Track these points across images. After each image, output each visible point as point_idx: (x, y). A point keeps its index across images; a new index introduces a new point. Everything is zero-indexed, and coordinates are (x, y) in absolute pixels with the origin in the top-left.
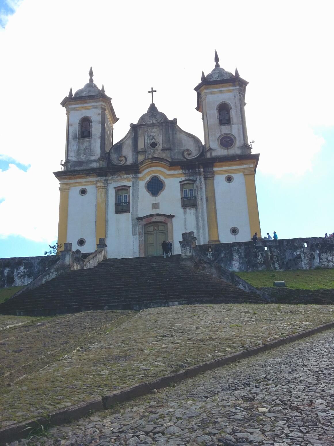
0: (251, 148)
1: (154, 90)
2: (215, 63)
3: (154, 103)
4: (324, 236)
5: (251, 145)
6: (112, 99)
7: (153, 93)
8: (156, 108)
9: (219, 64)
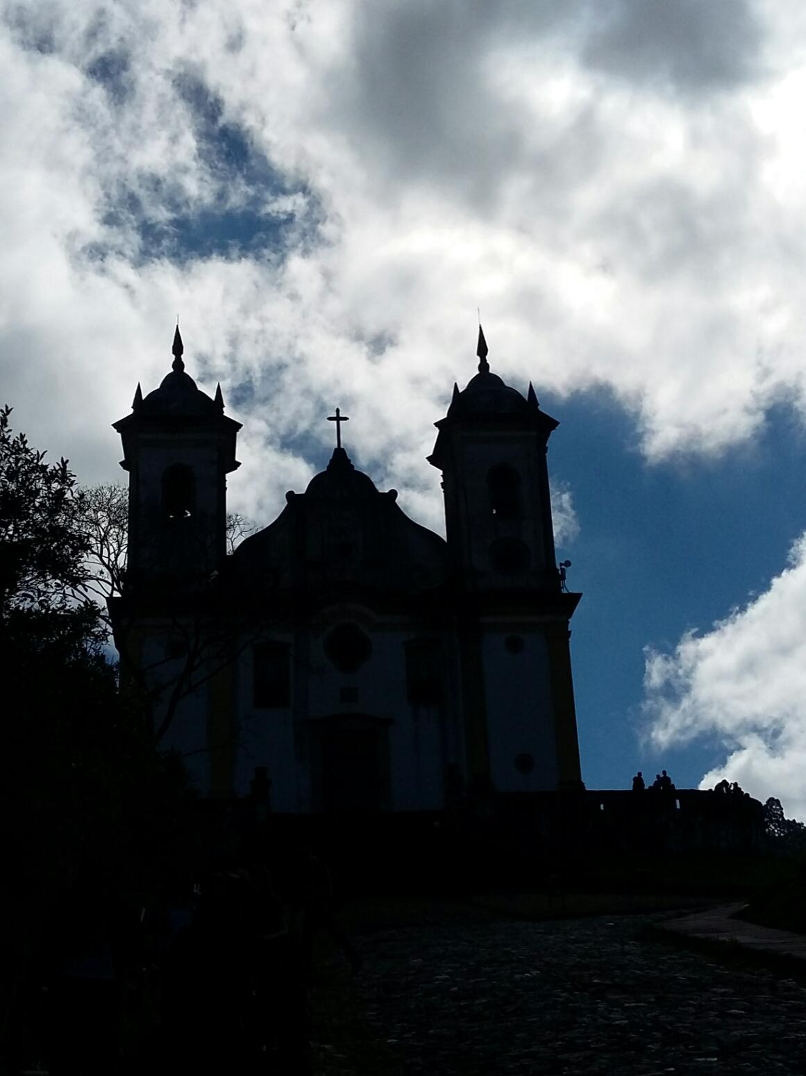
0: (563, 577)
1: (341, 415)
2: (173, 357)
3: (342, 447)
4: (629, 786)
5: (563, 570)
6: (556, 423)
7: (341, 422)
8: (350, 461)
9: (183, 360)
